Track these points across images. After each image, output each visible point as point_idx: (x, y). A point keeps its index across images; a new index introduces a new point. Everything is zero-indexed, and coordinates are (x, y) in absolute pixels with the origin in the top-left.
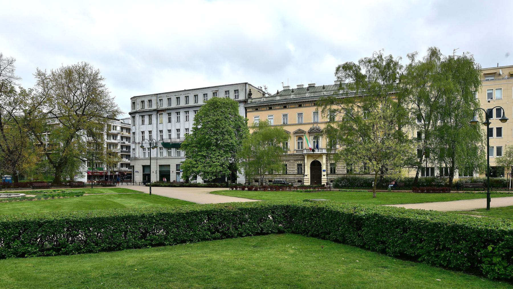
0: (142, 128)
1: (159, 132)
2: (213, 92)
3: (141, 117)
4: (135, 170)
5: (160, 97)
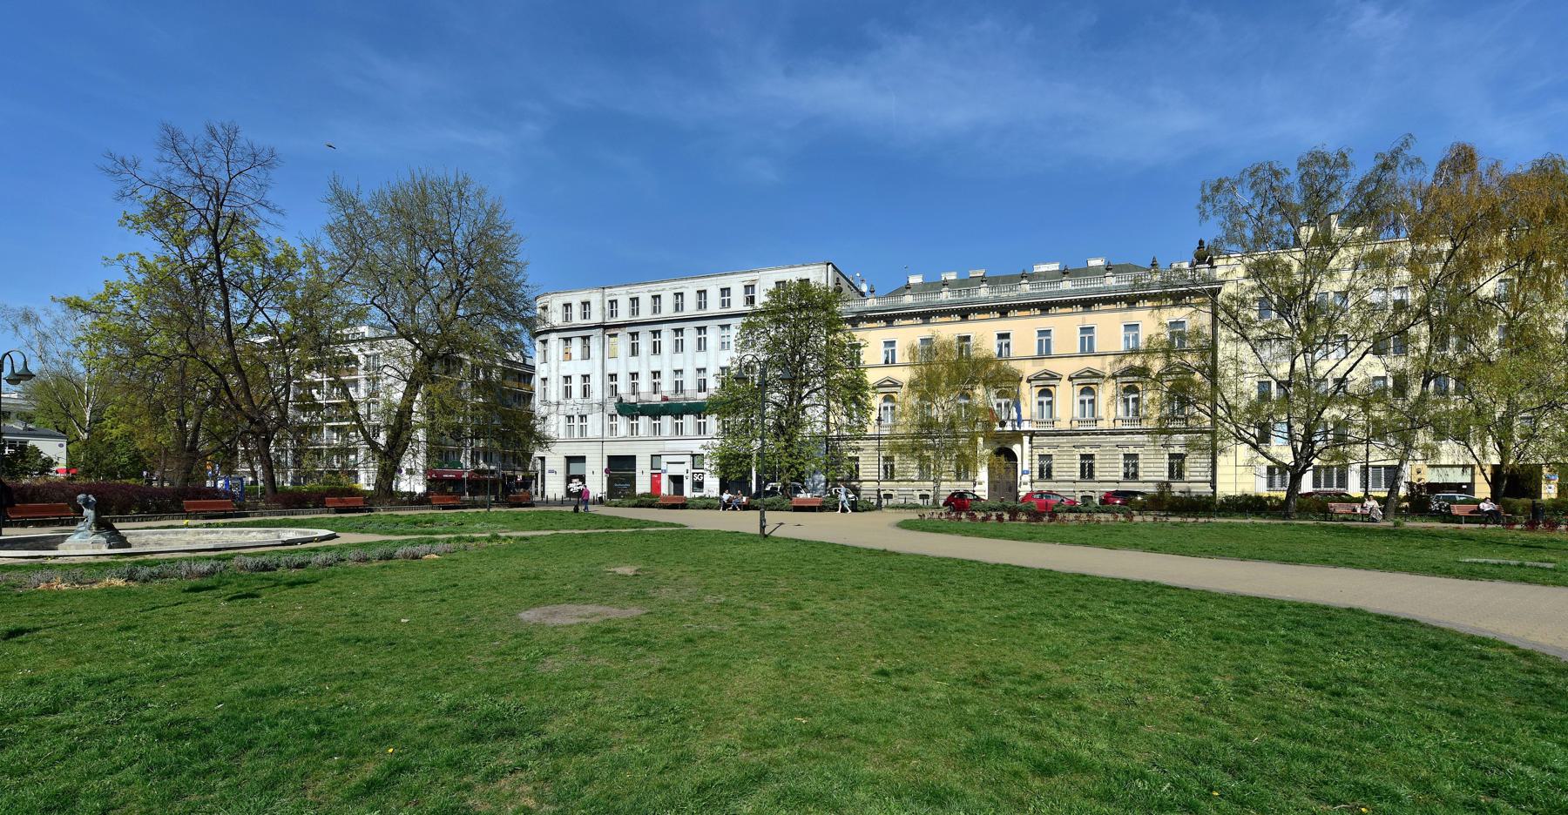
0: (565, 368)
1: (607, 378)
2: (746, 283)
3: (562, 341)
4: (547, 468)
5: (611, 295)
